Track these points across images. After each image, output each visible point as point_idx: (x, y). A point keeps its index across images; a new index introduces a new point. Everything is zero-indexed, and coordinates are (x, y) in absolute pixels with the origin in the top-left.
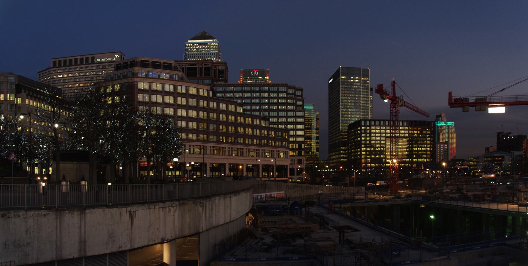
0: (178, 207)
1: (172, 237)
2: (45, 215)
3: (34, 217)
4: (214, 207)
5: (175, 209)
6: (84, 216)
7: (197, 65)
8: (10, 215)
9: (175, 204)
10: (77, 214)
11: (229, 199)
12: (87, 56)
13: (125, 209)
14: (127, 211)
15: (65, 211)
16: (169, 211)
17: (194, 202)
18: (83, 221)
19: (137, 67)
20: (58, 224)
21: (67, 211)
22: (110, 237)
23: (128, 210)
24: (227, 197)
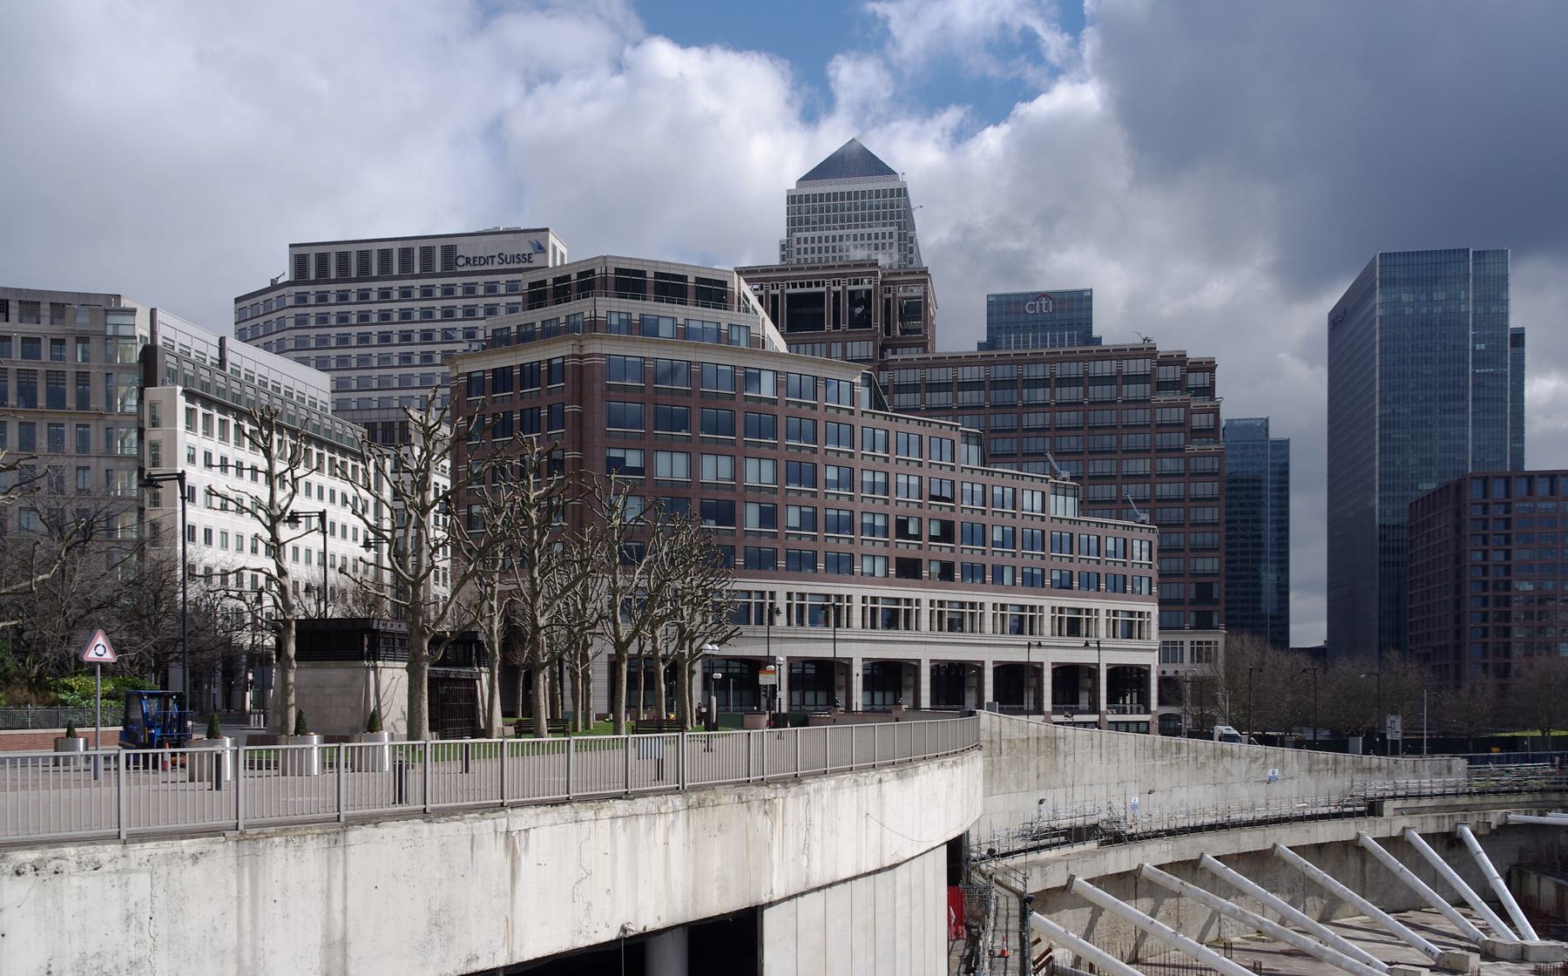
0: (682, 815)
1: (659, 918)
2: (195, 858)
3: (156, 866)
4: (817, 818)
5: (669, 823)
6: (340, 852)
7: (823, 282)
8: (63, 862)
9: (670, 803)
10: (315, 847)
11: (874, 789)
12: (425, 243)
13: (490, 822)
14: (496, 832)
15: (270, 840)
16: (650, 829)
17: (740, 797)
18: (340, 873)
19: (1505, 316)
20: (247, 885)
21: (277, 840)
22: (436, 925)
23: (501, 827)
24: (868, 782)
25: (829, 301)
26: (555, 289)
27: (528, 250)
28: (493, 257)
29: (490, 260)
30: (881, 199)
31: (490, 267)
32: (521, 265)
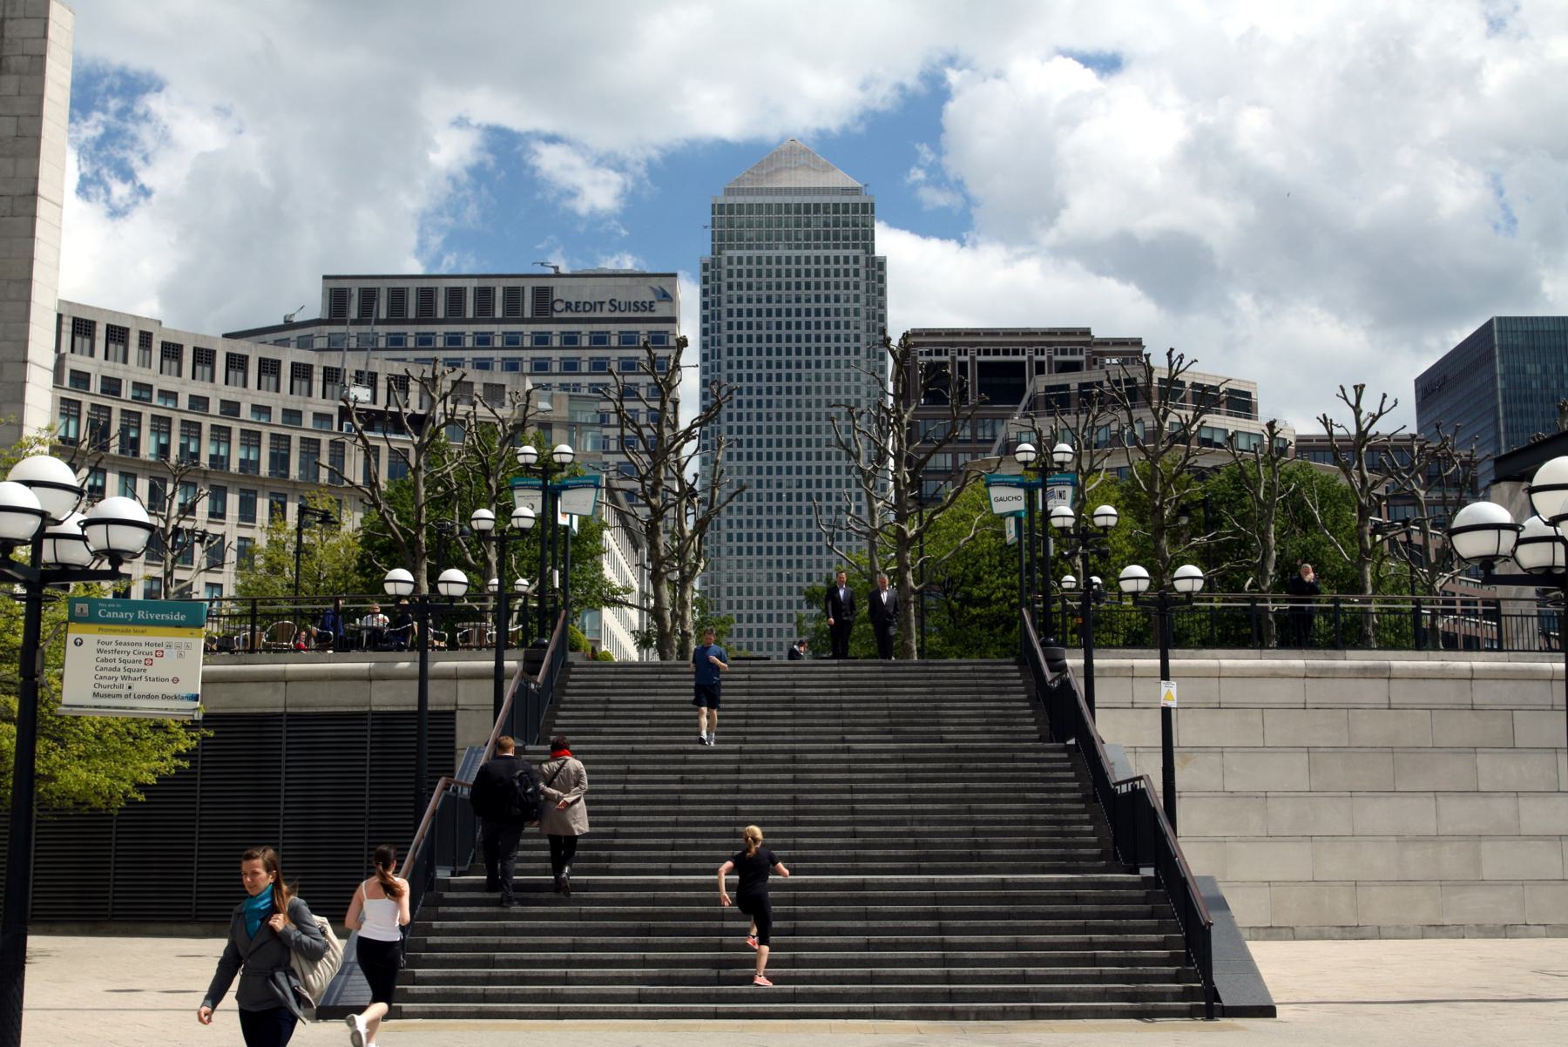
7: (1081, 351)
12: (512, 283)
25: (973, 374)
26: (1081, 394)
27: (648, 296)
28: (602, 303)
29: (598, 306)
30: (841, 215)
31: (598, 314)
32: (639, 314)
